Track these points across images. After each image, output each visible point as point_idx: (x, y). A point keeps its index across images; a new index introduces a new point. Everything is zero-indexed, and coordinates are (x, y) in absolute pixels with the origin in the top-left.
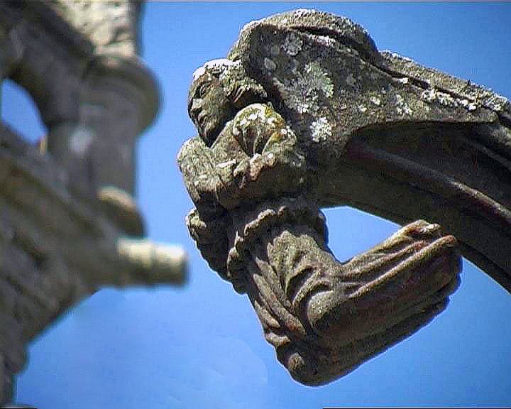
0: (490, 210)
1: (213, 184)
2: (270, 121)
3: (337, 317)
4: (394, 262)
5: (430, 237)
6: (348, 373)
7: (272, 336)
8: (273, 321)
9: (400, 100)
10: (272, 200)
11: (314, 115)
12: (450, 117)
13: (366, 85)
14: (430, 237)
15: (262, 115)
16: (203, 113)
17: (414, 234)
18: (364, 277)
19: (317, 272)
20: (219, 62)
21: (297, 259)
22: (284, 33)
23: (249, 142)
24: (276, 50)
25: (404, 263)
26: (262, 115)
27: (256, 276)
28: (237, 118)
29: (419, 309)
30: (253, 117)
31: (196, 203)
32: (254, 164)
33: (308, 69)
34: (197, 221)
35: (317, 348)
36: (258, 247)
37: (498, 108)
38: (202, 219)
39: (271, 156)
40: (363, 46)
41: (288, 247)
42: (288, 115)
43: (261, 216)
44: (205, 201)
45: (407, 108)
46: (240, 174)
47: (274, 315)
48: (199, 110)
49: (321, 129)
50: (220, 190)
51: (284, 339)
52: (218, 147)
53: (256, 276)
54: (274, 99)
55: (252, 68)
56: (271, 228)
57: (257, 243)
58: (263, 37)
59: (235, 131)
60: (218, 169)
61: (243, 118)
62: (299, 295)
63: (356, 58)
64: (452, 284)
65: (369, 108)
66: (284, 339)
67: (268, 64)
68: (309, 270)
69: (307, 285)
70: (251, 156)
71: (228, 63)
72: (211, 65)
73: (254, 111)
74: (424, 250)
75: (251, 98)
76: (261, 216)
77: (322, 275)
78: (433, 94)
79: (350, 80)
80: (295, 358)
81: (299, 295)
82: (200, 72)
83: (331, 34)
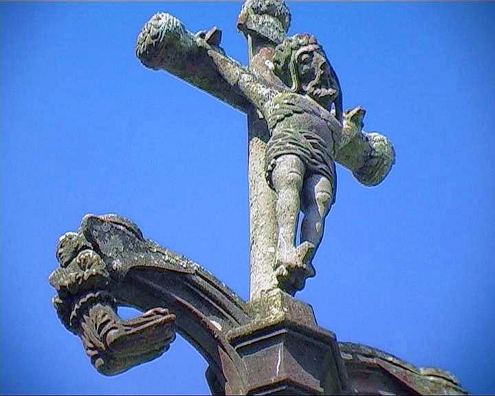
0: (190, 310)
1: (66, 283)
2: (94, 257)
3: (120, 342)
4: (147, 322)
5: (164, 314)
6: (211, 93)
7: (89, 351)
8: (91, 345)
9: (153, 258)
10: (93, 290)
11: (114, 258)
12: (173, 268)
13: (138, 250)
14: (164, 314)
15: (91, 254)
16: (64, 254)
17: (158, 313)
18: (134, 326)
19: (113, 321)
20: (71, 233)
21: (104, 316)
22: (103, 221)
23: (83, 265)
24: (98, 228)
25: (151, 323)
26: (91, 254)
27: (83, 324)
28: (79, 255)
29: (156, 347)
30: (87, 254)
31: (59, 291)
32: (86, 274)
33: (112, 238)
34: (58, 300)
35: (111, 356)
36: (86, 311)
37: (195, 268)
38: (60, 299)
39: (94, 270)
40: (139, 234)
41: (100, 311)
42: (103, 256)
43: (88, 296)
44: (63, 291)
45: (155, 262)
46: (79, 278)
47: (91, 342)
48: (60, 254)
49: (117, 264)
50: (69, 285)
51: (96, 352)
52: (68, 268)
53: (83, 324)
54: (96, 248)
55: (88, 235)
56: (93, 301)
57: (84, 309)
58: (93, 220)
59: (78, 261)
60: (70, 276)
61: (82, 255)
62: (103, 331)
63: (134, 236)
64: (168, 340)
65: (140, 259)
66: (96, 352)
67: (95, 233)
68: (108, 321)
69: (108, 327)
70: (85, 270)
71: (77, 235)
72: (68, 234)
73: (88, 252)
74: (160, 320)
75: (85, 247)
76: (88, 296)
77: (115, 323)
78: (167, 258)
79: (131, 246)
80: (100, 361)
81: (103, 331)
82: (63, 237)
83: (124, 226)
